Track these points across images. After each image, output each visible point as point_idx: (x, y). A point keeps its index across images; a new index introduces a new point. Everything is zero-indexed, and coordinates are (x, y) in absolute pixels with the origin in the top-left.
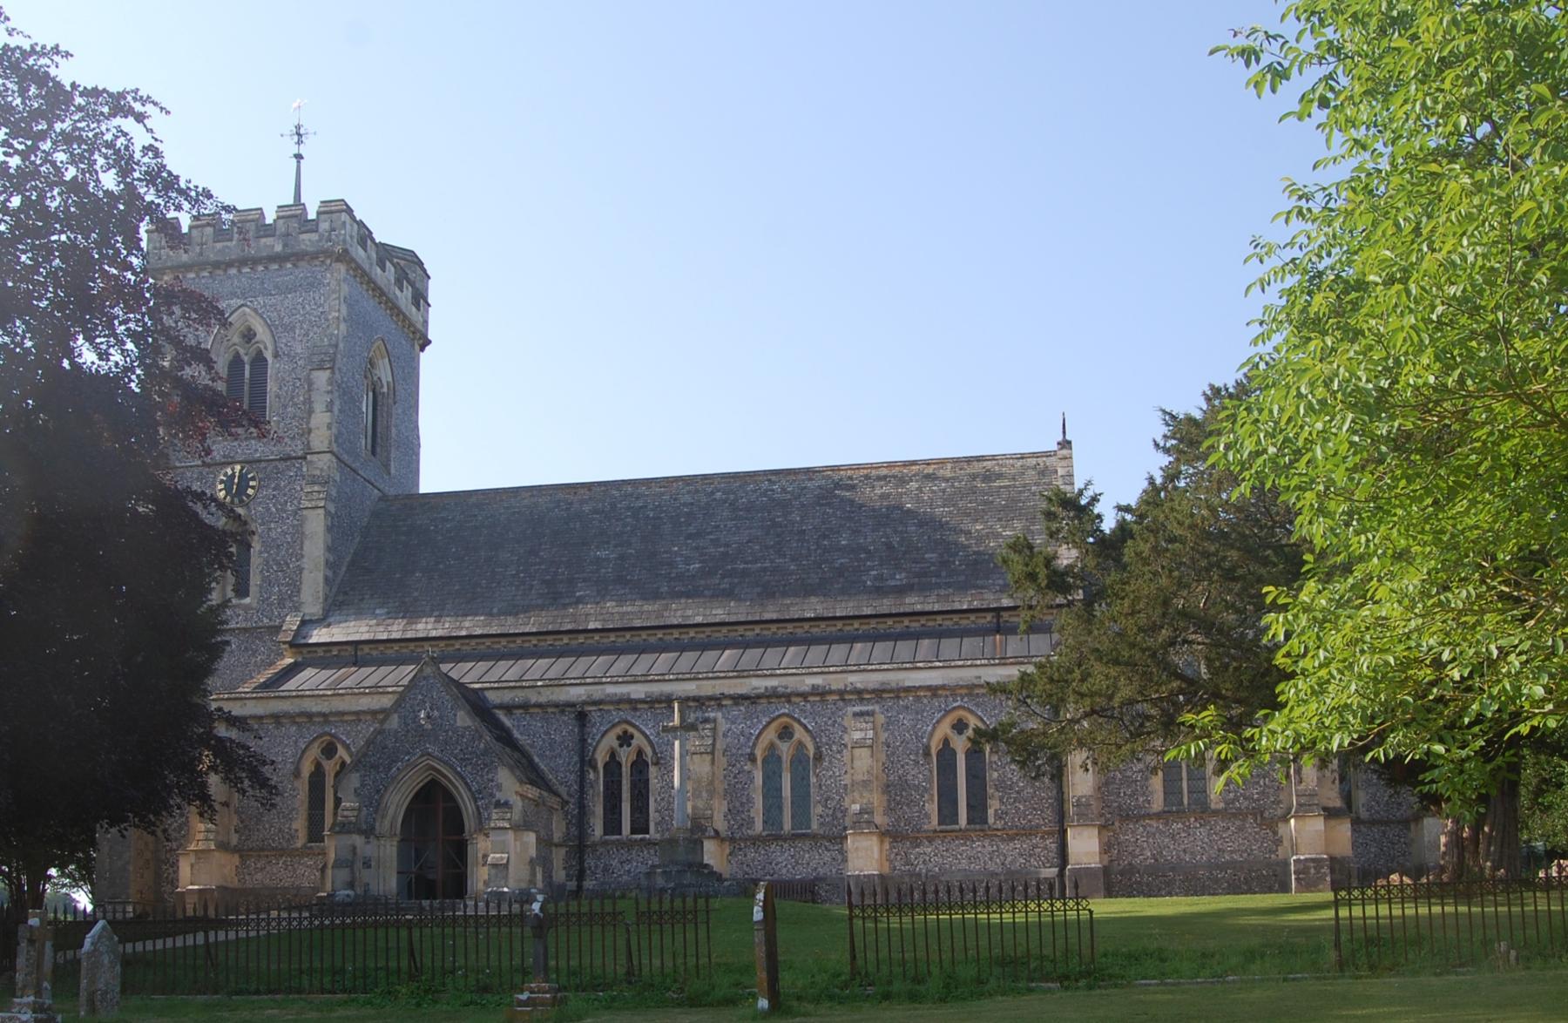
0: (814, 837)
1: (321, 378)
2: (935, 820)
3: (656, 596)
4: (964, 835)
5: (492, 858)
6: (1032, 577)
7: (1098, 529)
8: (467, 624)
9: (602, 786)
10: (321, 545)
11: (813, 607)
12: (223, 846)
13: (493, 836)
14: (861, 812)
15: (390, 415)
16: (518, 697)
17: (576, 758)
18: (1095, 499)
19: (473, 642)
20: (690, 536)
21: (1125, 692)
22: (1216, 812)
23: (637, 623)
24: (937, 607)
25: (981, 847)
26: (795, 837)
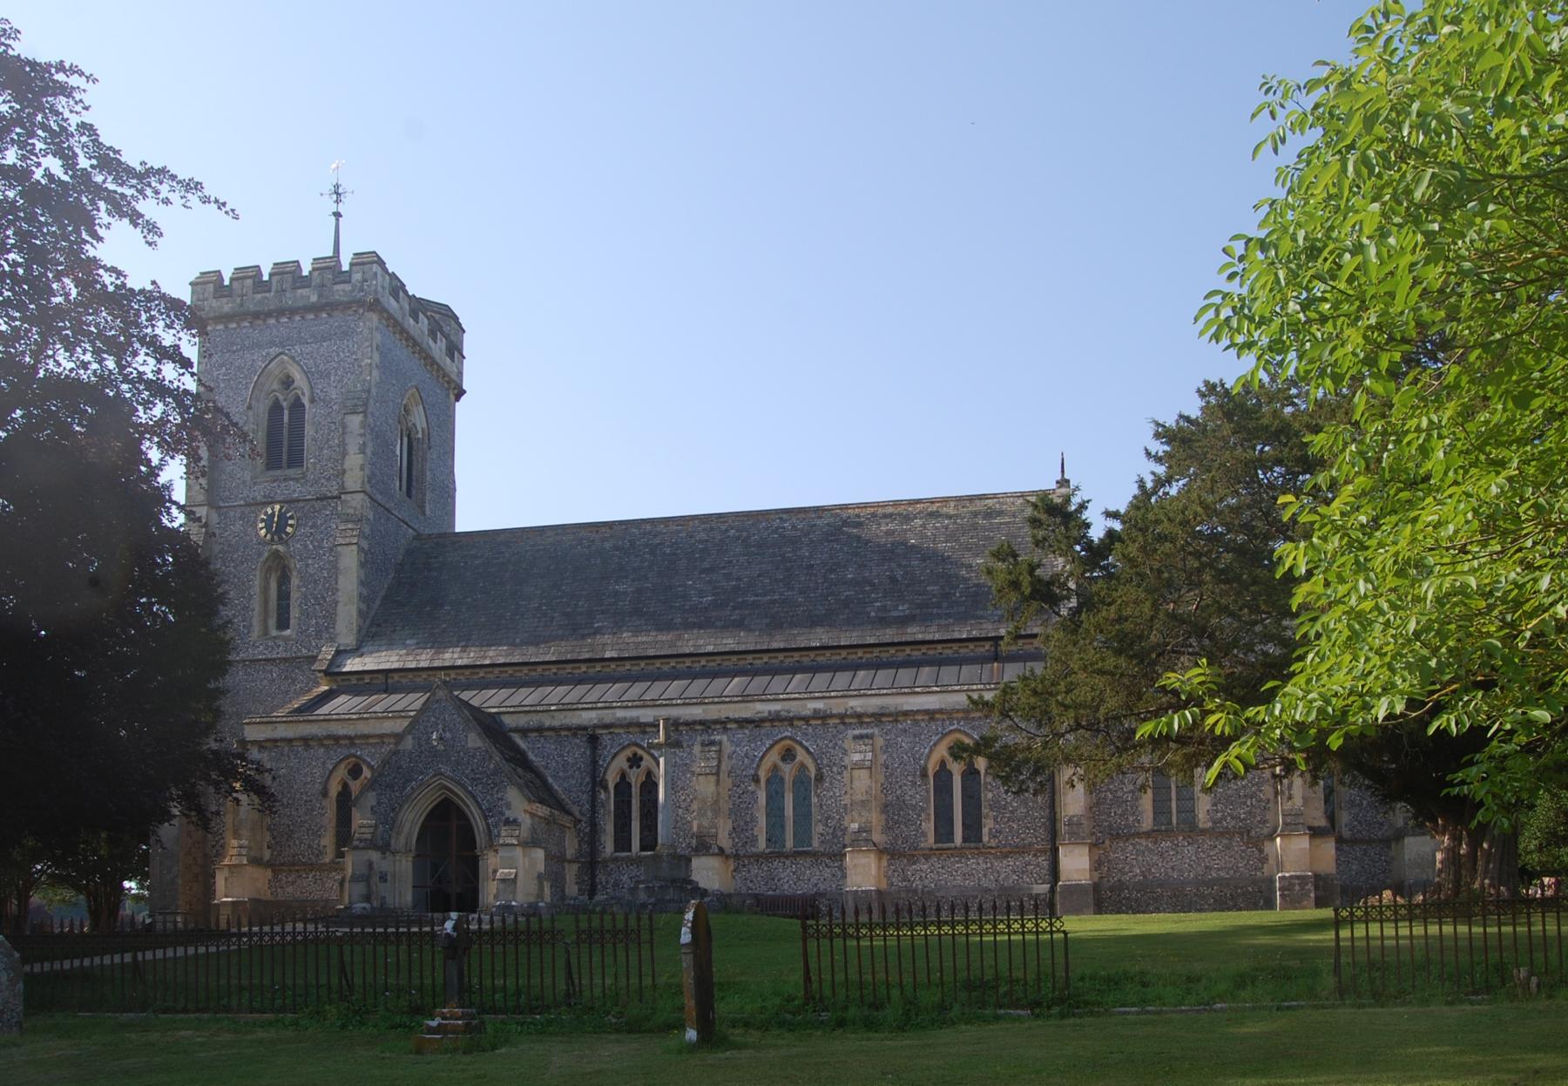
0: (814, 855)
1: (355, 421)
2: (931, 838)
3: (668, 627)
4: (960, 853)
5: (502, 872)
6: (1015, 585)
7: (1085, 536)
8: (491, 654)
9: (607, 806)
10: (355, 580)
11: (819, 637)
12: (256, 861)
13: (502, 852)
14: (860, 831)
15: (424, 459)
16: (533, 720)
17: (588, 779)
18: (1083, 506)
19: (496, 670)
20: (703, 571)
21: (1112, 703)
22: (1204, 832)
23: (651, 652)
24: (937, 637)
25: (976, 864)
26: (797, 854)
